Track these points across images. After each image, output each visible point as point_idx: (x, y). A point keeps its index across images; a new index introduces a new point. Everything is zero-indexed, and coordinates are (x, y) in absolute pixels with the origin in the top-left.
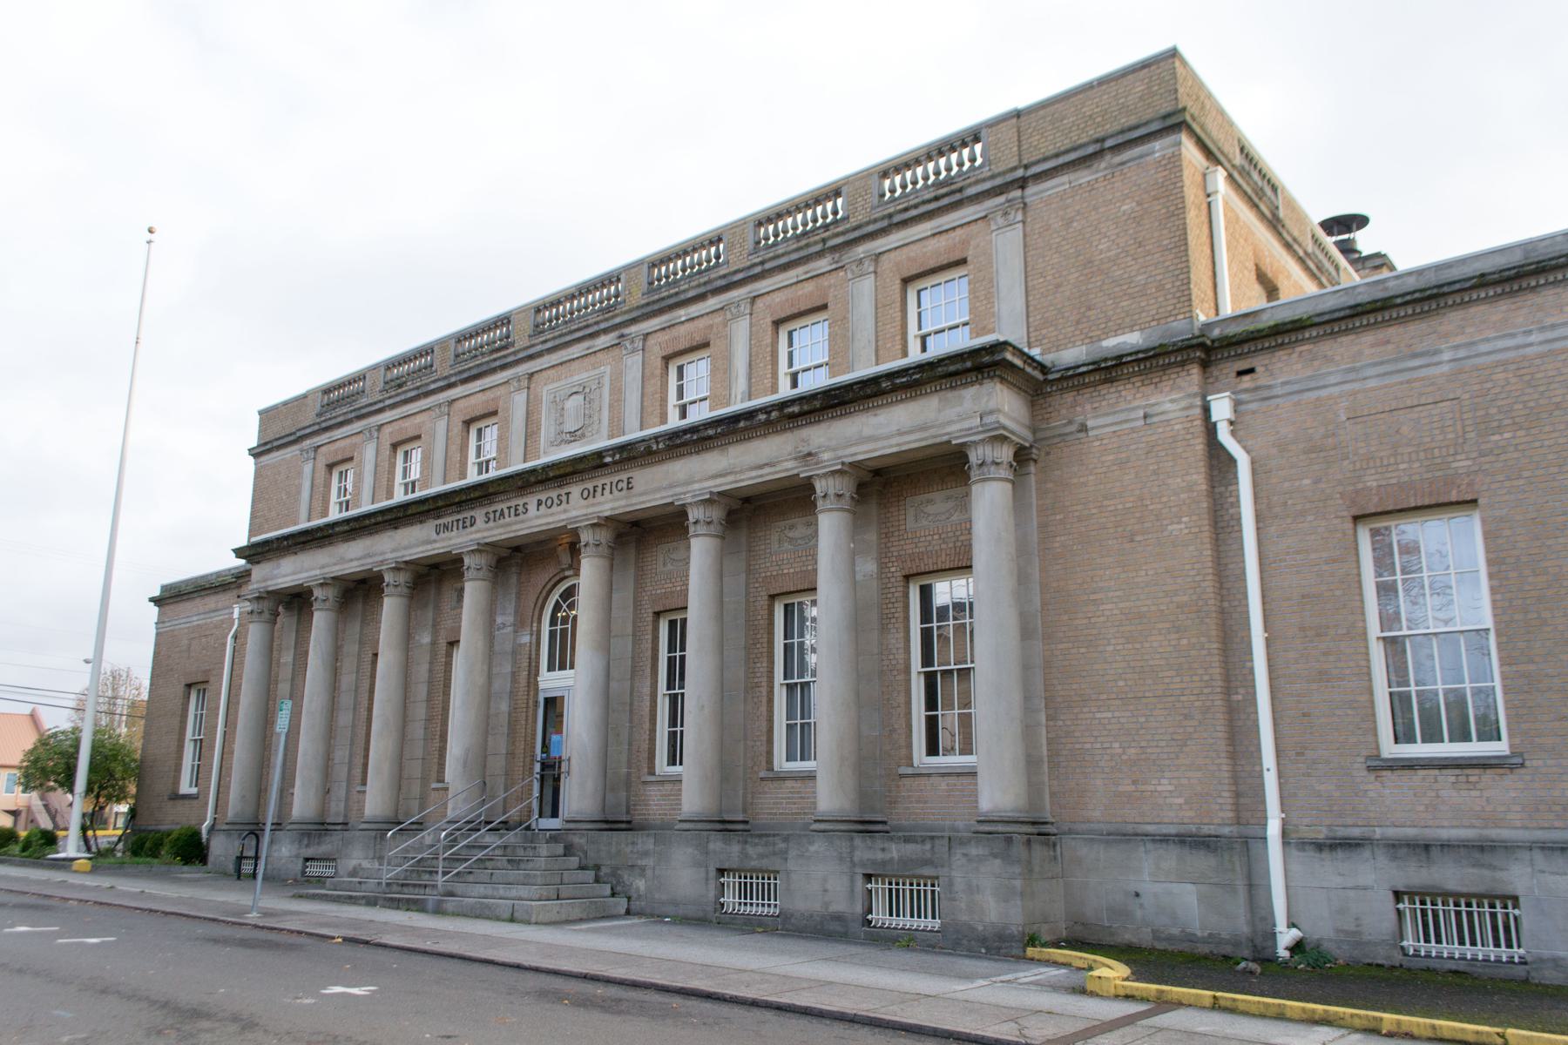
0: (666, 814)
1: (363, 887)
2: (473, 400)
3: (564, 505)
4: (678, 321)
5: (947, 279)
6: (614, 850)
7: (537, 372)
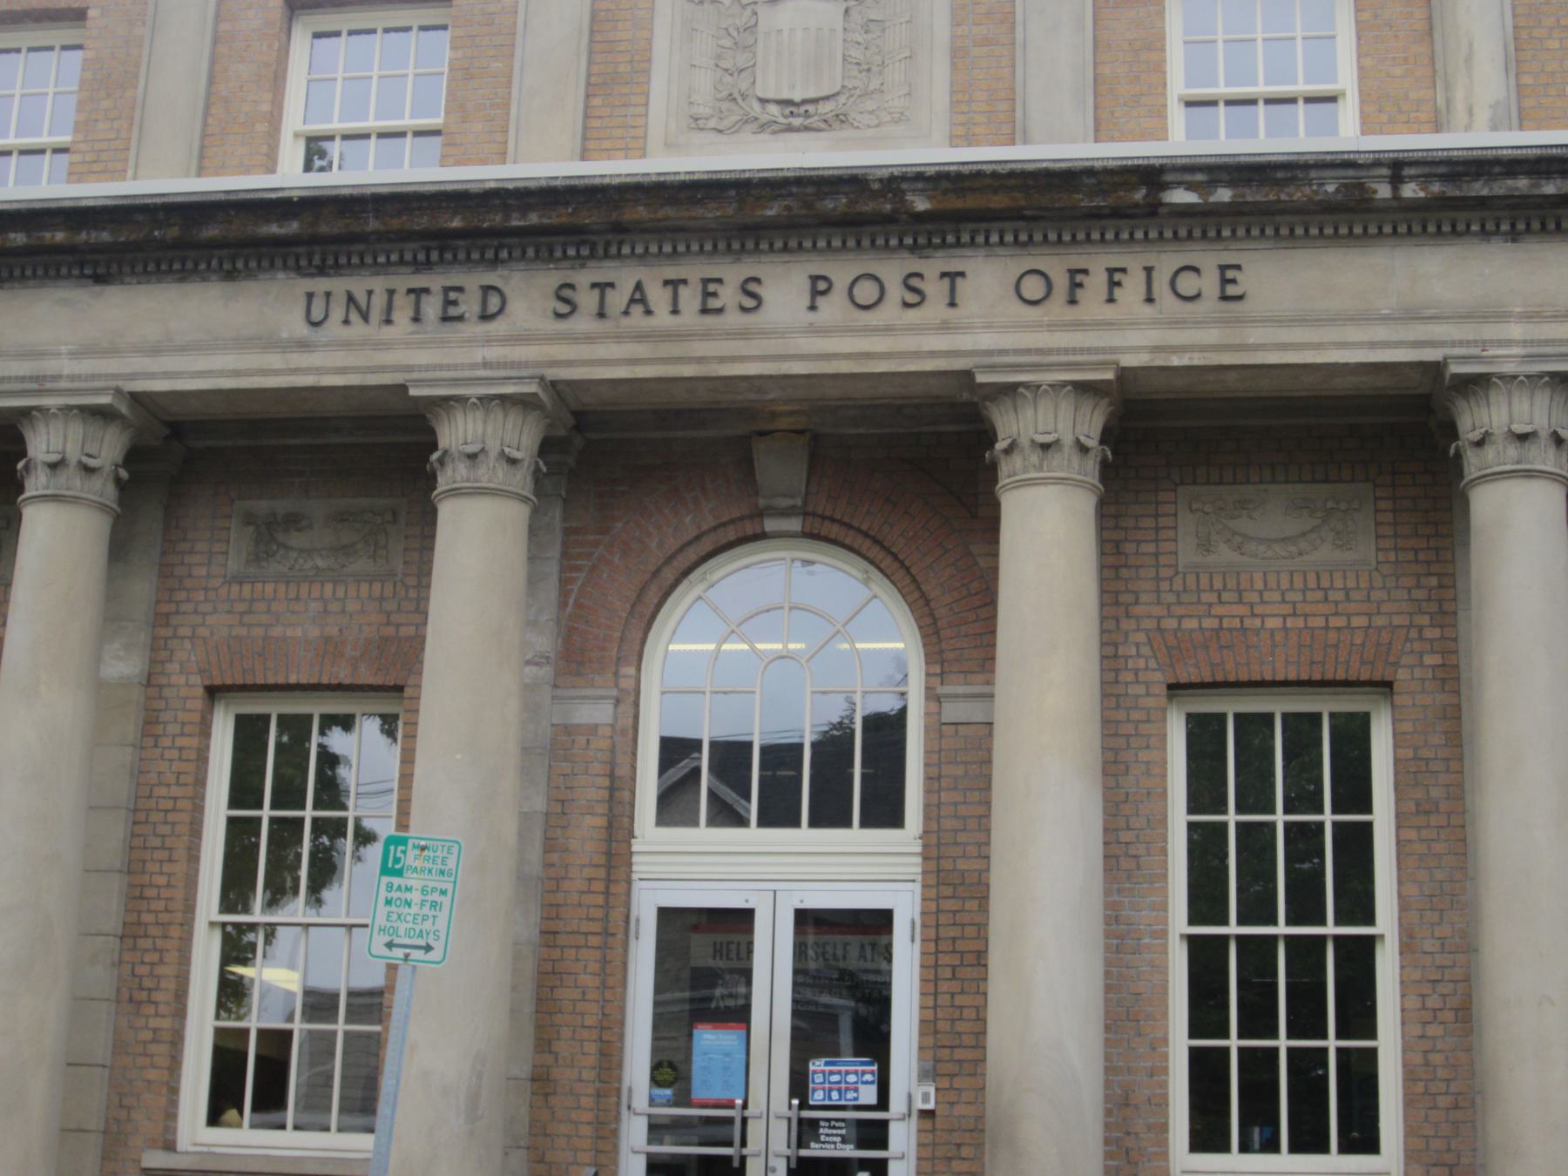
3: (935, 309)
5: (354, 26)
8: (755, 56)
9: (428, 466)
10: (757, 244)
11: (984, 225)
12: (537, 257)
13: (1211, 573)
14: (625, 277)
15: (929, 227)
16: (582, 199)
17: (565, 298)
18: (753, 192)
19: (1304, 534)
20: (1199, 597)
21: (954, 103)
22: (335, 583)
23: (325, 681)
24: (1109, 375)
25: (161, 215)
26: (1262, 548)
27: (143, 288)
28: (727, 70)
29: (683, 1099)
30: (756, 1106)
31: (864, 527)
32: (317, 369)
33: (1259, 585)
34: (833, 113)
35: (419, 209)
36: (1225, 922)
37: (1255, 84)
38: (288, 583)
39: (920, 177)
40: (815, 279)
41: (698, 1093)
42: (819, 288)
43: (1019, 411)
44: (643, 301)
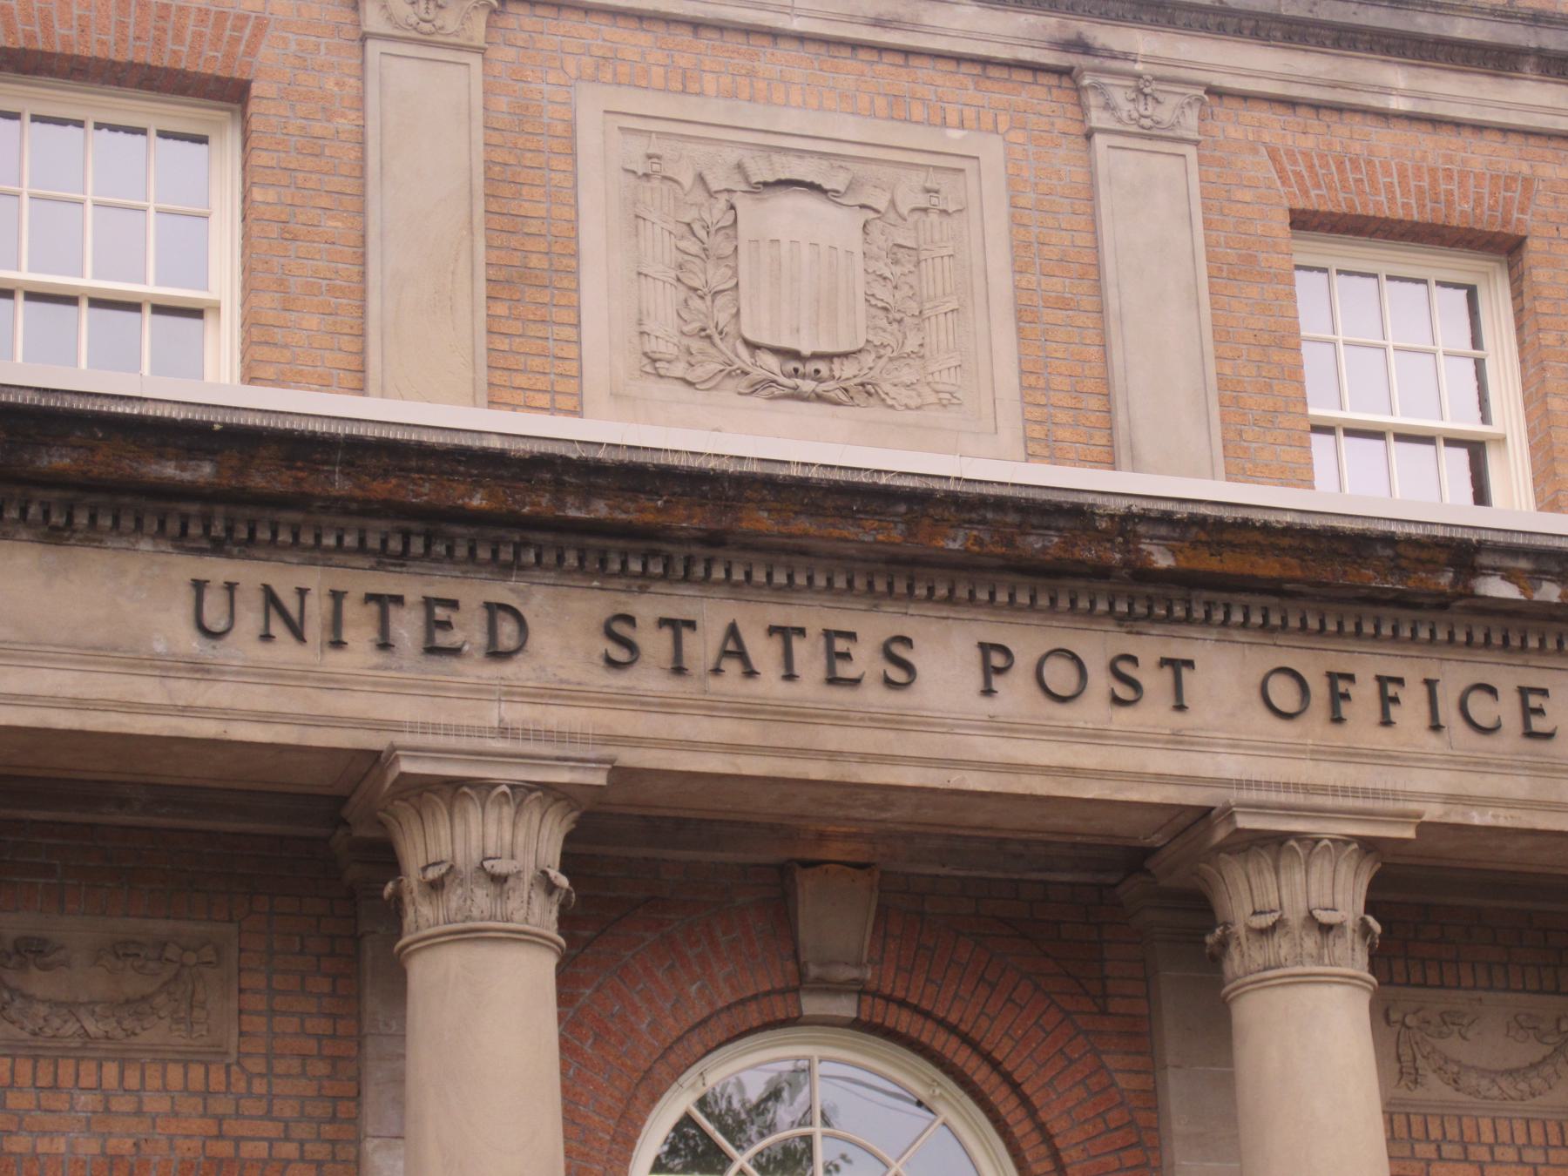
3: (1154, 713)
8: (735, 273)
10: (910, 588)
11: (1225, 596)
13: (1425, 1116)
15: (1150, 590)
16: (678, 490)
17: (618, 631)
18: (931, 511)
20: (1413, 1148)
21: (1025, 389)
22: (123, 1064)
26: (1485, 1083)
28: (695, 290)
31: (953, 1018)
32: (224, 710)
33: (1488, 1137)
34: (858, 380)
35: (420, 470)
38: (36, 1058)
39: (1166, 518)
40: (986, 648)
43: (1282, 872)
44: (741, 655)
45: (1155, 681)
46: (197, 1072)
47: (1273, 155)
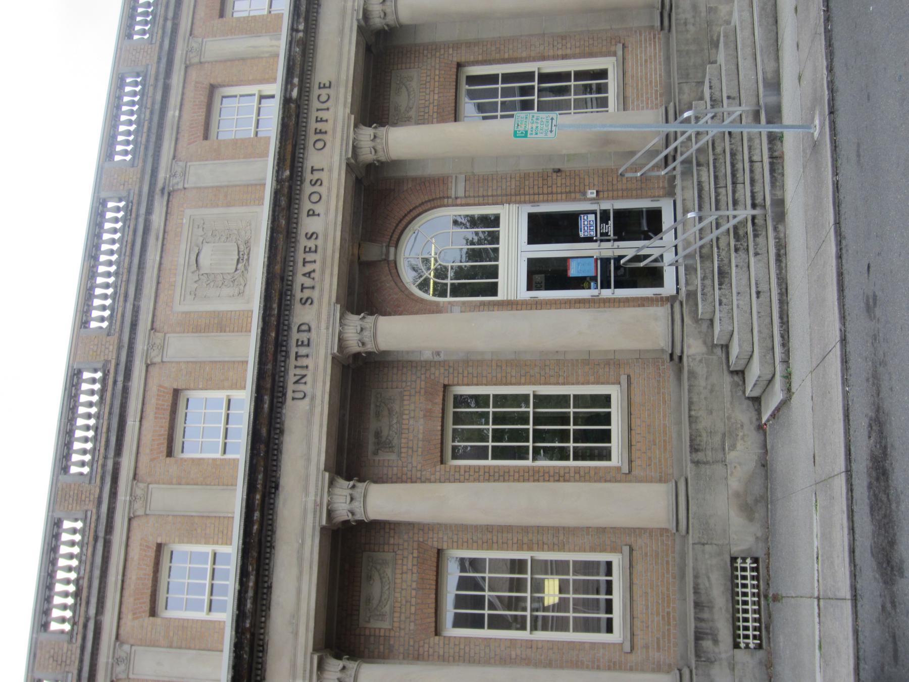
0: (656, 91)
1: (763, 287)
2: (147, 438)
3: (324, 176)
4: (177, 119)
6: (693, 47)
7: (153, 322)
9: (364, 355)
12: (289, 310)
14: (300, 279)
19: (407, 90)
21: (246, 205)
23: (441, 415)
24: (327, 474)
25: (255, 452)
27: (283, 467)
29: (594, 279)
30: (596, 254)
31: (395, 225)
33: (423, 101)
36: (528, 447)
37: (222, 413)
39: (278, 172)
40: (308, 215)
41: (592, 274)
42: (312, 213)
44: (310, 273)
45: (316, 176)
46: (406, 398)
47: (189, 144)
